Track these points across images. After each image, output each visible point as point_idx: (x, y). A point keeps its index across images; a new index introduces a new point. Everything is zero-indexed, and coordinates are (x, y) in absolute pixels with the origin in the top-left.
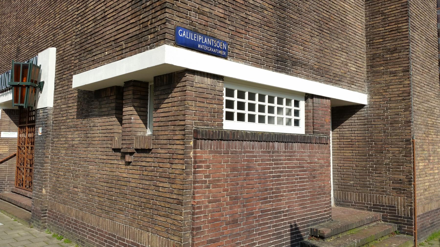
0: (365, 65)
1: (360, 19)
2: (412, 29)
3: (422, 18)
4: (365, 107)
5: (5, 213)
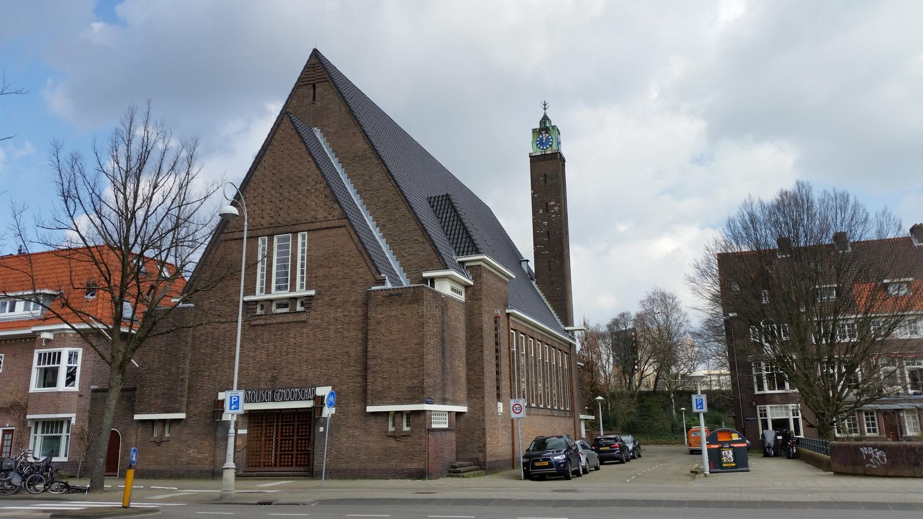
4: (465, 415)
5: (396, 292)
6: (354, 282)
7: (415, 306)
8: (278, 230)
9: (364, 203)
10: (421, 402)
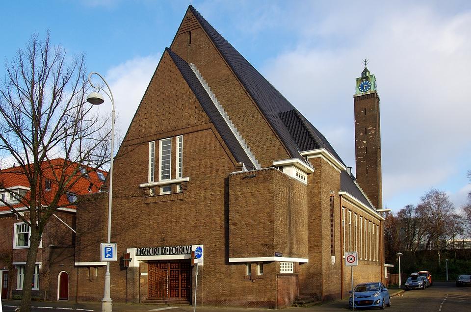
6: (218, 170)
7: (266, 184)
8: (162, 136)
9: (228, 115)
10: (271, 255)
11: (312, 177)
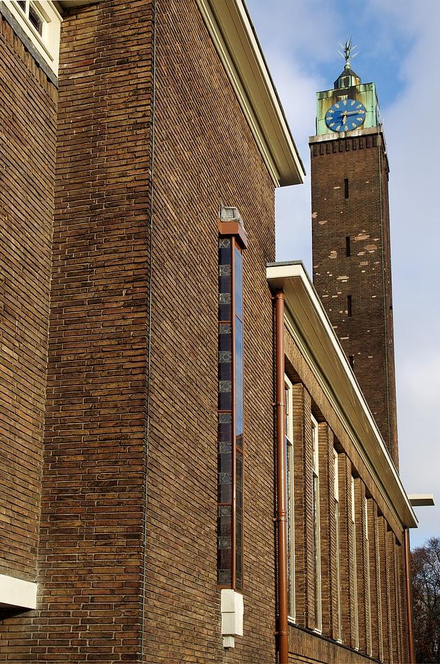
0: (39, 511)
1: (30, 400)
2: (154, 443)
3: (180, 422)
4: (31, 614)
11: (90, 32)
